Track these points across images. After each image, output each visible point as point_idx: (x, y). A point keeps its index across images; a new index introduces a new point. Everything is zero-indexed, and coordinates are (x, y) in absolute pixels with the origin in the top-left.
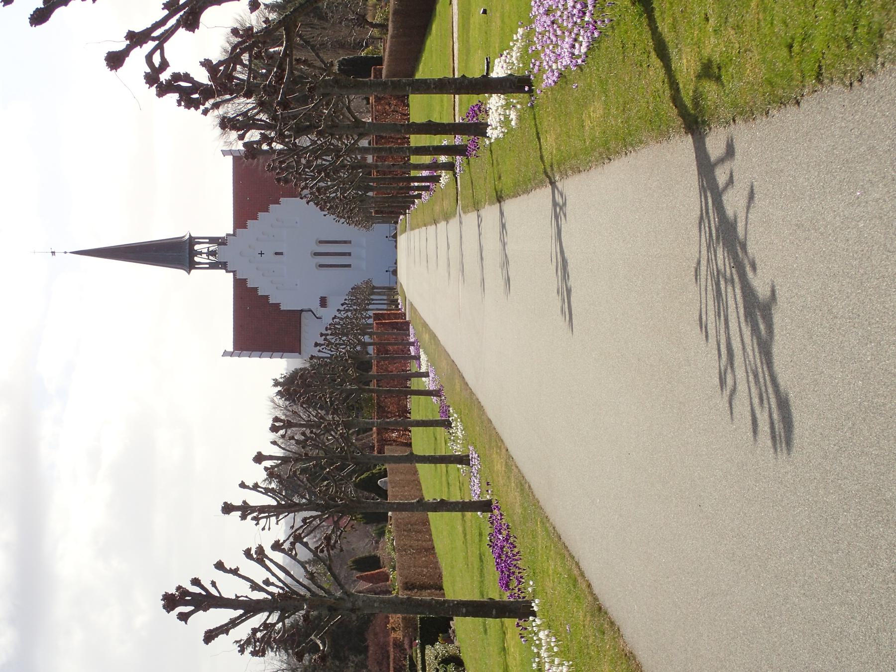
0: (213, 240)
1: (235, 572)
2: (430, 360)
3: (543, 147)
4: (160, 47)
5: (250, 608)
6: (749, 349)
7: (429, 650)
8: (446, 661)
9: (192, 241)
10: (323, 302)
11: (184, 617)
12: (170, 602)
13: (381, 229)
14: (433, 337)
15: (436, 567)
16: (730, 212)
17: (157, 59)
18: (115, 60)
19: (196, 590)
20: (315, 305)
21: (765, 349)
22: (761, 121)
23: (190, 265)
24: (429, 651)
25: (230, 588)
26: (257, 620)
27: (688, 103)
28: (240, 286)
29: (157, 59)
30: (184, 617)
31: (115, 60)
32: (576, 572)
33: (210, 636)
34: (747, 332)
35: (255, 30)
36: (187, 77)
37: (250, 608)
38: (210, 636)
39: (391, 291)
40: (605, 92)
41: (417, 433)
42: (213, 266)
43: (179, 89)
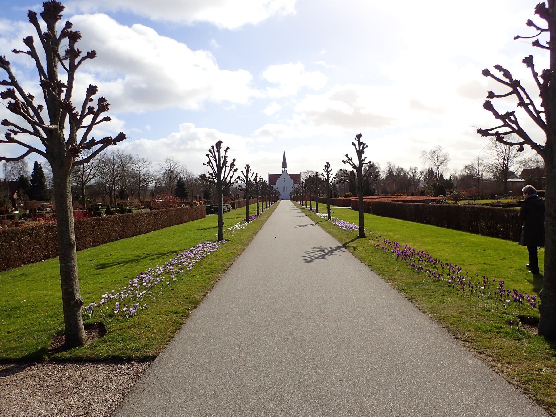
0: (287, 171)
1: (252, 176)
2: (274, 205)
3: (206, 231)
4: (348, 162)
5: (247, 178)
6: (317, 255)
7: (231, 206)
8: (229, 209)
9: (286, 168)
10: (277, 188)
11: (245, 168)
12: (247, 166)
13: (289, 197)
14: (277, 205)
15: (242, 207)
16: (334, 252)
17: (346, 162)
18: (347, 156)
19: (250, 169)
20: (277, 187)
21: (317, 258)
22: (354, 257)
23: (283, 167)
24: (231, 206)
25: (250, 175)
26: (245, 179)
27: (348, 245)
28: (280, 175)
29: (346, 162)
30: (245, 168)
31: (347, 156)
32: (259, 229)
33: (242, 172)
34: (318, 255)
35: (448, 179)
36: (329, 167)
37: (247, 178)
38: (242, 172)
39: (280, 199)
40: (338, 232)
41: (261, 203)
42: (283, 171)
43: (327, 165)
